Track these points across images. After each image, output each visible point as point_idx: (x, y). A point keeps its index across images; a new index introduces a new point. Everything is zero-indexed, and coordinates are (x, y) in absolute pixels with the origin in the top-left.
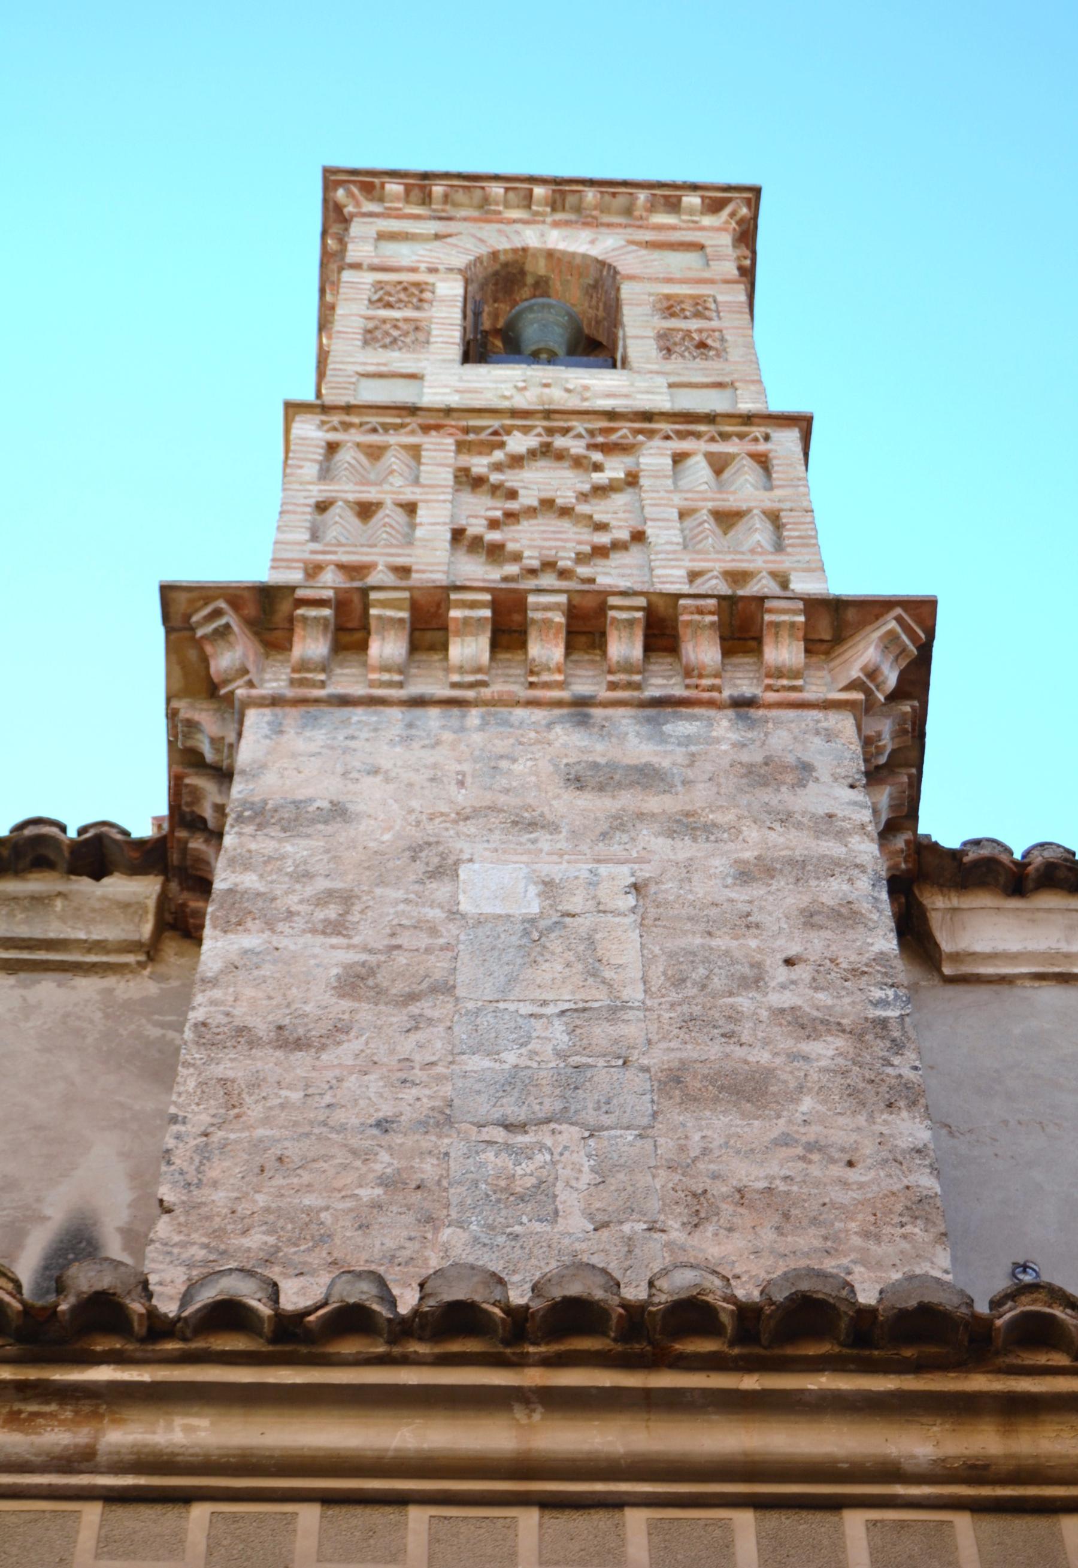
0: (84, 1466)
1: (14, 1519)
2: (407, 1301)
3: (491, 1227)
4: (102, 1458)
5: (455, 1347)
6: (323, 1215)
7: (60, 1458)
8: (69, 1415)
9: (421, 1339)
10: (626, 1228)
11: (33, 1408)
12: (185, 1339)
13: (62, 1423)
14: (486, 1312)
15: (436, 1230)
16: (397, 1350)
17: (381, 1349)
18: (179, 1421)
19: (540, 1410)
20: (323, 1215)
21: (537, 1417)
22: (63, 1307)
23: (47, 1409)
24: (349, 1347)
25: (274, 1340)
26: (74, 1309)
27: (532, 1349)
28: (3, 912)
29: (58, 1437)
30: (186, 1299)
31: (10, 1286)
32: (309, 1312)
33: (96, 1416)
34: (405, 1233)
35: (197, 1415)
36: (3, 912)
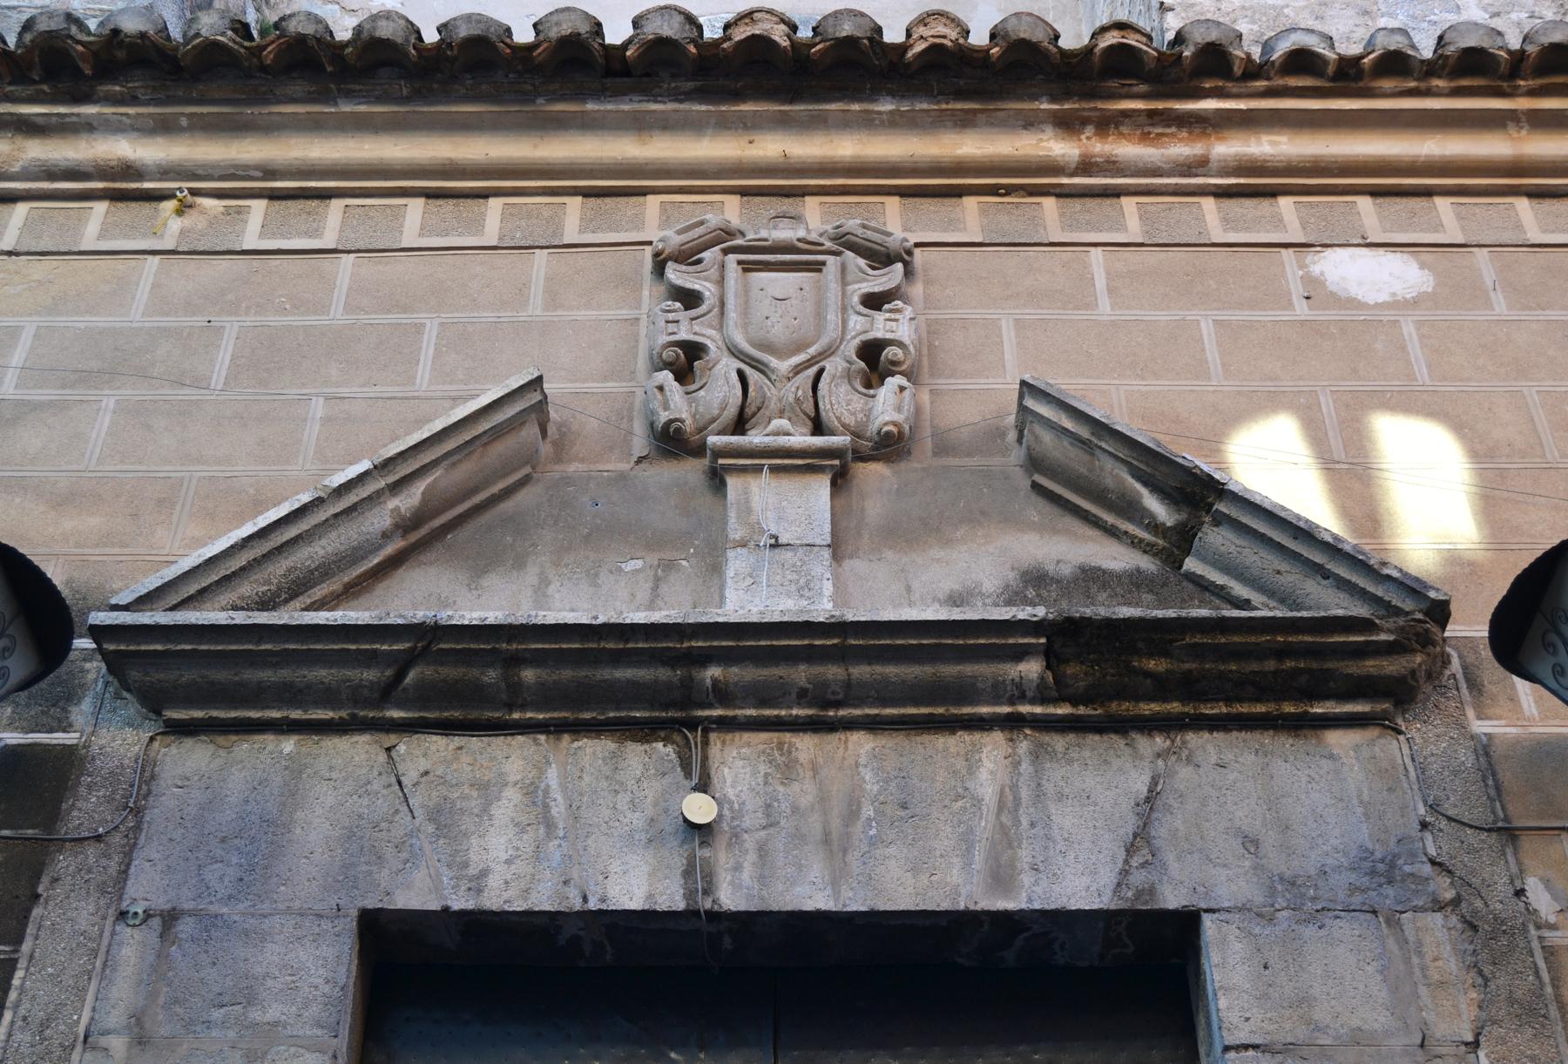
0: (1200, 171)
1: (1153, 208)
2: (1426, 49)
3: (1414, 17)
4: (1213, 165)
5: (1465, 82)
6: (1286, 11)
7: (1182, 165)
8: (1185, 134)
9: (1440, 77)
10: (1514, 16)
11: (1160, 130)
12: (1268, 79)
13: (1181, 140)
14: (1493, 55)
15: (1373, 19)
16: (1423, 85)
17: (1413, 84)
18: (1265, 138)
19: (1527, 127)
20: (1286, 11)
21: (1524, 132)
22: (1187, 53)
23: (1168, 131)
24: (1387, 84)
25: (1333, 79)
26: (1196, 55)
27: (1522, 83)
28: (3, 806)
29: (1181, 149)
30: (1267, 46)
31: (1144, 39)
32: (1363, 57)
33: (1204, 134)
34: (1351, 22)
35: (1278, 134)
36: (3, 806)
